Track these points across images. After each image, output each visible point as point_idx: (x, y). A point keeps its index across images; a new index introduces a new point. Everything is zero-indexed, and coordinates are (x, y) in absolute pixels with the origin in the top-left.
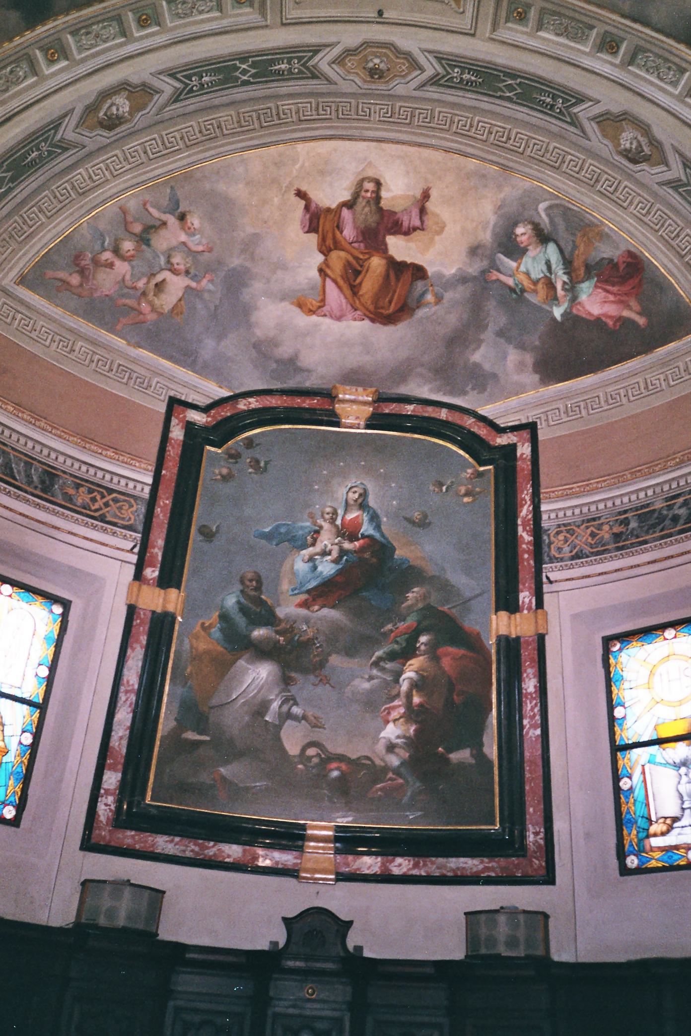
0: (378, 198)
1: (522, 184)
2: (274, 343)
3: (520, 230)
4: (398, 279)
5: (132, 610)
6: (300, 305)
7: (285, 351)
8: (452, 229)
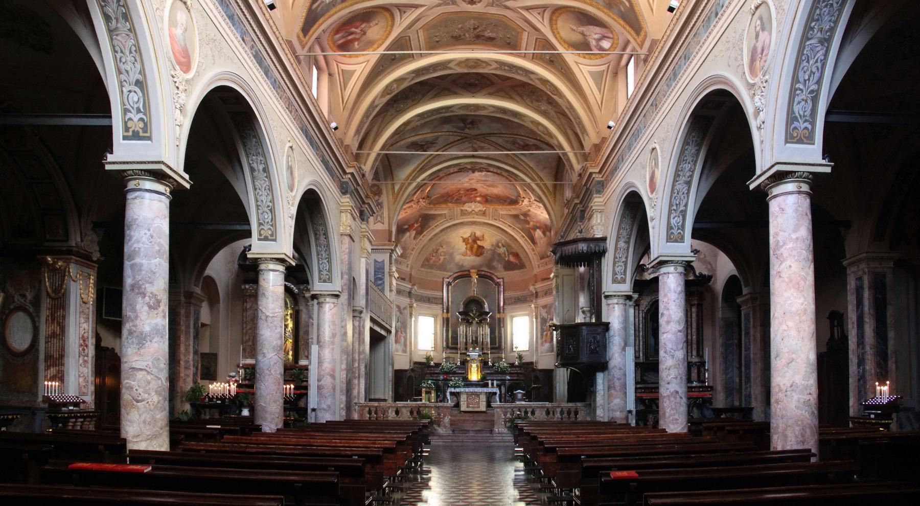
1: (498, 238)
5: (443, 318)
7: (461, 263)
8: (488, 241)
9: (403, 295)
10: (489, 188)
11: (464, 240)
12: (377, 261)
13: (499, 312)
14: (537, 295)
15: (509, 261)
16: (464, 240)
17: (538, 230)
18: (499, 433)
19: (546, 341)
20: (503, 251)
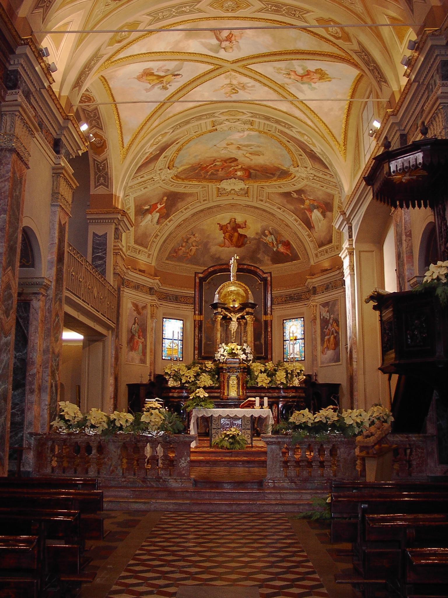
0: (235, 222)
1: (265, 224)
2: (215, 255)
3: (266, 232)
4: (241, 237)
5: (195, 321)
6: (220, 246)
7: (217, 256)
9: (142, 291)
10: (252, 157)
11: (222, 228)
12: (97, 235)
13: (266, 313)
14: (315, 291)
15: (278, 252)
16: (222, 228)
17: (315, 211)
18: (274, 488)
19: (328, 348)
20: (270, 240)
